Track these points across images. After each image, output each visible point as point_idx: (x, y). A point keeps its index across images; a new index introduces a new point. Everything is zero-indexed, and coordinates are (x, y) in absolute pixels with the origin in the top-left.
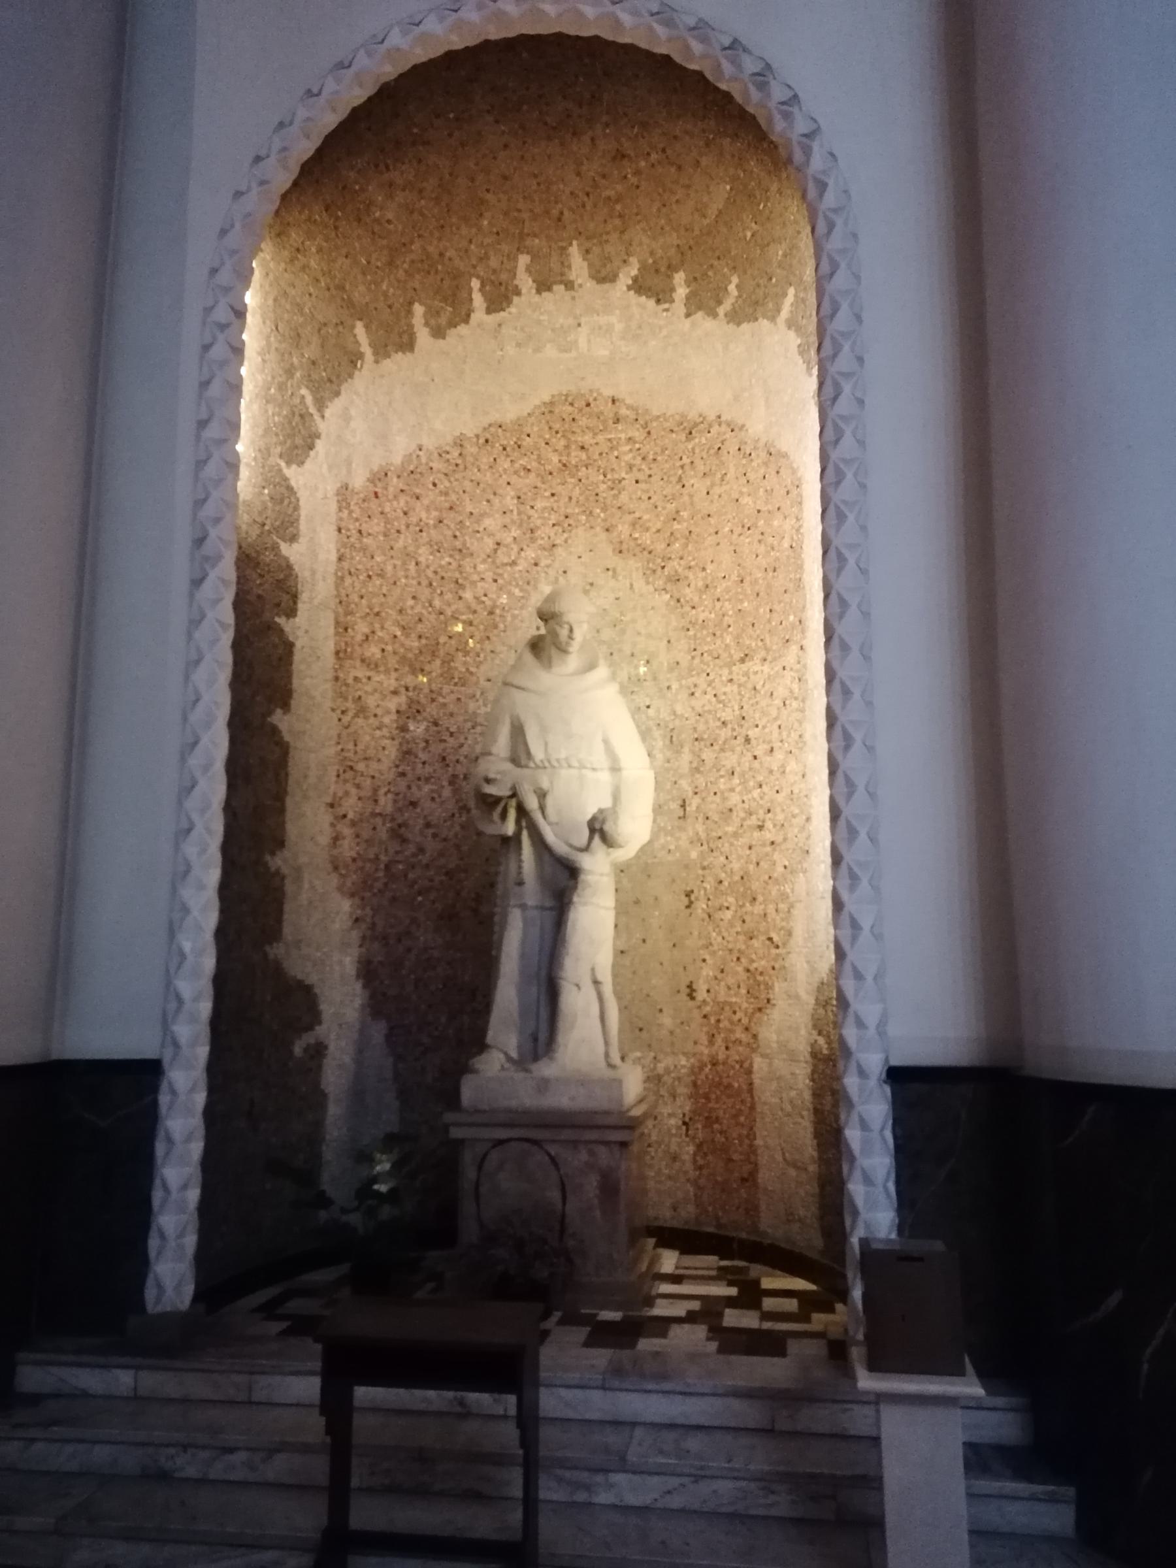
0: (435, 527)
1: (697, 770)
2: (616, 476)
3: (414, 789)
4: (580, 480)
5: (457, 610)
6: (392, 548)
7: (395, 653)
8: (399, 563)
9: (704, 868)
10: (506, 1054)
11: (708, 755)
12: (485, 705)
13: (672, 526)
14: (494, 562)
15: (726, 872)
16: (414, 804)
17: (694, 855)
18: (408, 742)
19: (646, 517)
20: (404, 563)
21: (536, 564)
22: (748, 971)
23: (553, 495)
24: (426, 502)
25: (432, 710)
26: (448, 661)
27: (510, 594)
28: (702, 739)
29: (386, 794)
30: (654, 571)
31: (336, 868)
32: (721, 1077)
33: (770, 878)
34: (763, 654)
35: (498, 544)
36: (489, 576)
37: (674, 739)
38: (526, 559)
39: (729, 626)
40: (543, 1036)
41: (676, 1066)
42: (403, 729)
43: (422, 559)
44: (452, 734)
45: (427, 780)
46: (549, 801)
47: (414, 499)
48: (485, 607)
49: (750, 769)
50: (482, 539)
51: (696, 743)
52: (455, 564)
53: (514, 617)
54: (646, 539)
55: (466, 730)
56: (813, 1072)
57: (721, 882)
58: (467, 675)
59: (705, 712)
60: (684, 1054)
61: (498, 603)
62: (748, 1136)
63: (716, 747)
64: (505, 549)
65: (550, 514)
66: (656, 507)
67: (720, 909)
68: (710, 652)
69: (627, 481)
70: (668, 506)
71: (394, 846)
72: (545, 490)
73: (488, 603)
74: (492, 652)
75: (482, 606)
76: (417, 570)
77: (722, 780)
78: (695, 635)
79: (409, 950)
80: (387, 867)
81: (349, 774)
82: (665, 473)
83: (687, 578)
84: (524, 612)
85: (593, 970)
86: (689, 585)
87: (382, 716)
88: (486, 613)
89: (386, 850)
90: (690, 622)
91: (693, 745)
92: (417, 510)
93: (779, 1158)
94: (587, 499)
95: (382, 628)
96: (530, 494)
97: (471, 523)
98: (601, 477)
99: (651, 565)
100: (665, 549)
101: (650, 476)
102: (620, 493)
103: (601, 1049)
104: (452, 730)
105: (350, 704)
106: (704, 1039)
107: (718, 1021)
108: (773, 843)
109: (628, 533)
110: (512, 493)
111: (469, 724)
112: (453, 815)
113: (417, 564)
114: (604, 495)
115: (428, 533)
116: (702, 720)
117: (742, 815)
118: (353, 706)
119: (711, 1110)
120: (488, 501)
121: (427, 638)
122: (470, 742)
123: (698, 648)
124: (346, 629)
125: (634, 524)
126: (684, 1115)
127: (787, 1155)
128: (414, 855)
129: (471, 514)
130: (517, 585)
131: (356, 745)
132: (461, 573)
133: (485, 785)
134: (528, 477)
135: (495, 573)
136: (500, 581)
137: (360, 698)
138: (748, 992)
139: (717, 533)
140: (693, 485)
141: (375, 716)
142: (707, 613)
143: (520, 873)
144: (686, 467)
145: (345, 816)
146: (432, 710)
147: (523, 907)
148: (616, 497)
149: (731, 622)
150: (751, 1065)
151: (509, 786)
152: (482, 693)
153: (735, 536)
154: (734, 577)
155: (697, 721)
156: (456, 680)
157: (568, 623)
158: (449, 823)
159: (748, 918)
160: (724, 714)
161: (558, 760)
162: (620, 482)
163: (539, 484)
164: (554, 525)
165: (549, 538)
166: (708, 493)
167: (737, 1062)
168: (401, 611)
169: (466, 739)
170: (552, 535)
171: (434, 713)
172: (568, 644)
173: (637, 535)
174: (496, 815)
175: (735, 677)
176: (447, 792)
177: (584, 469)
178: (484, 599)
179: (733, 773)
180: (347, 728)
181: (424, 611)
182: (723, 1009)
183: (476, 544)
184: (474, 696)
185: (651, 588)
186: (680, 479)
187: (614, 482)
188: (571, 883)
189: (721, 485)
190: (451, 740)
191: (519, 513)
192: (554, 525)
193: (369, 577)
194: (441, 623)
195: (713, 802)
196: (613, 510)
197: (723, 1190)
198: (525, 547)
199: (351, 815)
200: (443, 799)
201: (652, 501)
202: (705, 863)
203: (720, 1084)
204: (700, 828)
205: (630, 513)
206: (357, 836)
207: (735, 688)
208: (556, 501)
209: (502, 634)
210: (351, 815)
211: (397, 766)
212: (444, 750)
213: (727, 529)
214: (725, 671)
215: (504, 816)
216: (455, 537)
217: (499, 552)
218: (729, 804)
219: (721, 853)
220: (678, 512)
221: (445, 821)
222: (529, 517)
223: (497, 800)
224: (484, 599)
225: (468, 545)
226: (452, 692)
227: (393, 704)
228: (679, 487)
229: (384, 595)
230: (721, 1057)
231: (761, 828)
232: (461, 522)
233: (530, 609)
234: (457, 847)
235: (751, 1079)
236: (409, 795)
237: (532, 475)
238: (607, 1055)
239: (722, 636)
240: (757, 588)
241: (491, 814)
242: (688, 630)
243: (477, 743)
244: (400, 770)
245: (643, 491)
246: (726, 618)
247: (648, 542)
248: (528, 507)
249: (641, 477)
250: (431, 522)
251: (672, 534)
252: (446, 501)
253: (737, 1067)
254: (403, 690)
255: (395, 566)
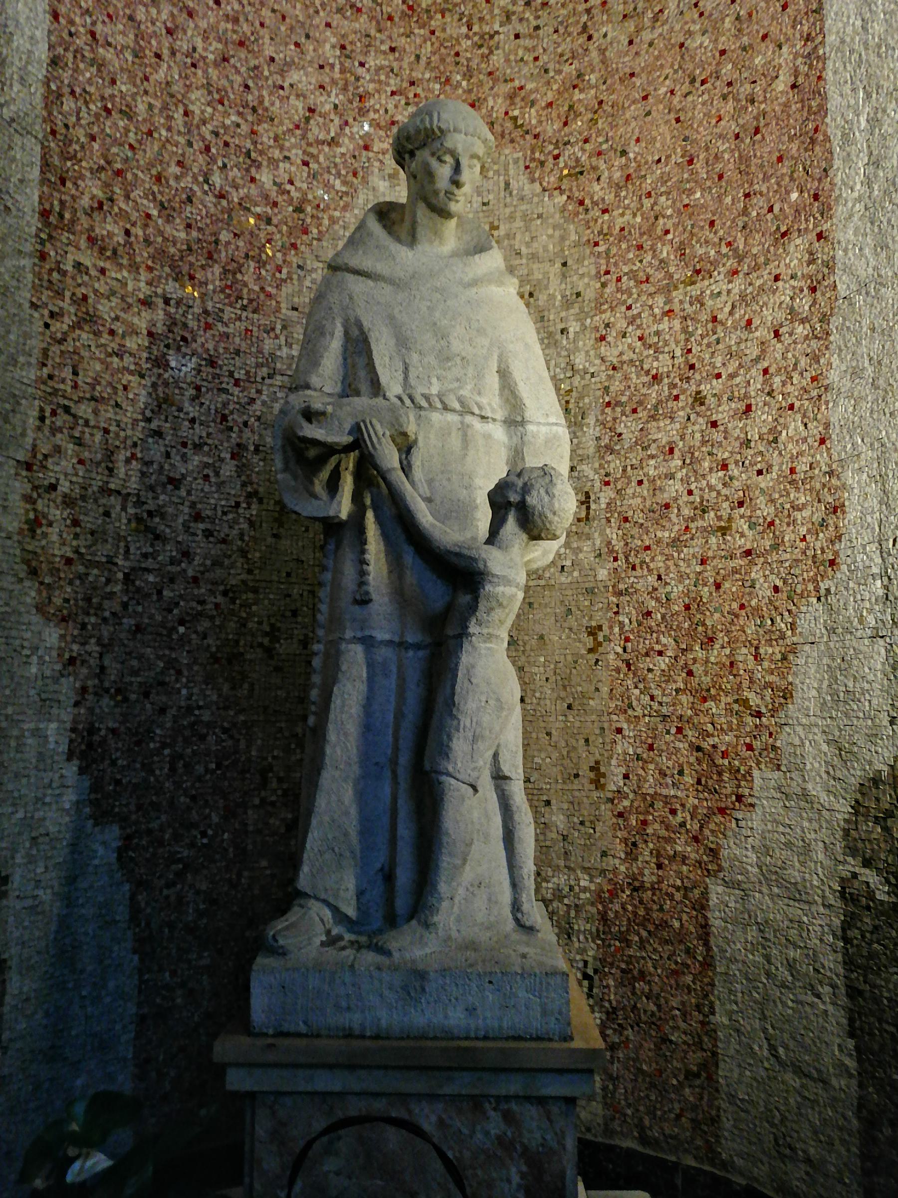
0: (216, 64)
1: (609, 449)
2: (487, 29)
3: (176, 459)
4: (433, 33)
5: (247, 196)
6: (147, 79)
7: (147, 241)
8: (158, 104)
9: (620, 594)
10: (335, 910)
11: (629, 428)
12: (290, 345)
13: (572, 96)
14: (304, 137)
15: (657, 600)
16: (175, 483)
17: (603, 574)
18: (166, 384)
19: (530, 86)
20: (165, 107)
21: (366, 148)
22: (699, 749)
23: (393, 50)
24: (203, 24)
25: (206, 341)
26: (232, 270)
27: (328, 187)
28: (618, 403)
29: (128, 461)
30: (542, 163)
31: (33, 572)
32: (648, 910)
33: (742, 607)
34: (731, 263)
35: (311, 110)
36: (297, 155)
37: (571, 406)
38: (352, 138)
39: (667, 232)
40: (404, 877)
41: (571, 888)
42: (160, 362)
43: (195, 108)
44: (237, 383)
45: (197, 447)
46: (417, 459)
47: (185, 15)
48: (290, 201)
49: (704, 442)
50: (288, 98)
51: (608, 410)
52: (245, 128)
53: (333, 221)
54: (531, 117)
55: (259, 379)
56: (846, 926)
57: (649, 613)
58: (262, 296)
59: (622, 363)
60: (585, 869)
61: (310, 197)
62: (698, 1007)
63: (642, 414)
64: (321, 120)
65: (388, 77)
66: (546, 71)
67: (647, 654)
68: (632, 275)
69: (502, 36)
70: (566, 68)
71: (139, 545)
72: (382, 42)
73: (295, 194)
74: (299, 267)
75: (285, 197)
76: (186, 123)
77: (652, 462)
78: (608, 252)
79: (163, 711)
80: (128, 579)
81: (62, 419)
82: (561, 23)
83: (595, 168)
84: (348, 215)
85: (496, 756)
86: (598, 179)
87: (123, 336)
88: (291, 209)
89: (127, 551)
90: (600, 233)
91: (603, 412)
92: (189, 33)
93: (761, 1049)
94: (443, 60)
95: (127, 197)
96: (358, 44)
97: (271, 74)
98: (464, 30)
99: (537, 155)
100: (560, 131)
101: (537, 28)
102: (491, 52)
103: (506, 897)
104: (236, 376)
105: (66, 304)
106: (620, 850)
107: (645, 823)
108: (748, 553)
109: (503, 110)
110: (333, 40)
111: (265, 371)
112: (238, 505)
113: (186, 114)
114: (469, 55)
115: (205, 72)
116: (619, 375)
117: (687, 512)
118: (72, 310)
119: (630, 960)
120: (297, 45)
121: (200, 229)
122: (264, 397)
123: (613, 269)
124: (63, 181)
125: (511, 97)
126: (586, 963)
127: (781, 1051)
128: (173, 561)
129: (272, 59)
130: (339, 174)
131: (75, 373)
132: (255, 143)
133: (305, 424)
134: (357, 20)
135: (304, 152)
136: (314, 166)
137: (85, 298)
138: (699, 782)
139: (645, 98)
140: (605, 36)
141: (112, 332)
142: (628, 217)
143: (362, 583)
144: (594, 11)
145: (53, 487)
146: (206, 341)
147: (368, 642)
148: (486, 57)
149: (669, 225)
150: (705, 894)
151: (347, 427)
152: (284, 327)
153: (676, 100)
154: (677, 158)
155: (609, 377)
156: (245, 302)
157: (453, 153)
158: (230, 516)
159: (698, 669)
160: (655, 364)
161: (427, 398)
162: (492, 37)
163: (373, 32)
164: (393, 93)
165: (386, 111)
166: (631, 42)
167: (678, 889)
168: (158, 179)
169: (259, 392)
170: (390, 107)
171: (210, 346)
172: (449, 194)
173: (516, 113)
174: (319, 487)
175: (676, 307)
176: (228, 469)
177: (439, 16)
178: (288, 187)
179: (671, 451)
180: (60, 342)
181: (195, 188)
182: (652, 805)
183: (277, 103)
184: (273, 329)
185: (537, 187)
186: (585, 27)
187: (482, 37)
188: (464, 599)
189: (653, 28)
190: (236, 391)
191: (343, 71)
192: (393, 93)
193: (108, 111)
194: (222, 212)
195: (634, 496)
196: (481, 77)
197: (652, 1085)
198: (351, 120)
199: (64, 487)
200: (222, 479)
201: (540, 63)
202: (622, 586)
203: (647, 919)
204: (613, 533)
205: (506, 81)
206: (76, 523)
207: (677, 324)
208: (396, 60)
209: (315, 242)
210: (64, 487)
211: (149, 420)
212: (225, 405)
213: (663, 90)
214: (660, 300)
215: (333, 486)
216: (247, 87)
217: (312, 122)
218: (665, 497)
219: (650, 570)
220: (580, 76)
221: (224, 513)
222: (358, 79)
223: (329, 450)
224: (288, 187)
225: (267, 104)
226: (239, 319)
227: (141, 320)
228: (582, 39)
229: (131, 147)
230: (649, 878)
231: (724, 531)
232: (256, 68)
233: (356, 211)
234: (244, 553)
235: (706, 918)
236: (167, 467)
237: (364, 18)
238: (516, 907)
239: (653, 249)
240: (719, 167)
241: (312, 483)
242: (596, 244)
243: (275, 400)
244: (154, 425)
245: (527, 49)
246: (661, 221)
247: (534, 122)
248: (357, 64)
249: (522, 29)
250: (211, 57)
251: (571, 107)
252: (234, 31)
253: (678, 896)
254: (160, 302)
255: (151, 107)
